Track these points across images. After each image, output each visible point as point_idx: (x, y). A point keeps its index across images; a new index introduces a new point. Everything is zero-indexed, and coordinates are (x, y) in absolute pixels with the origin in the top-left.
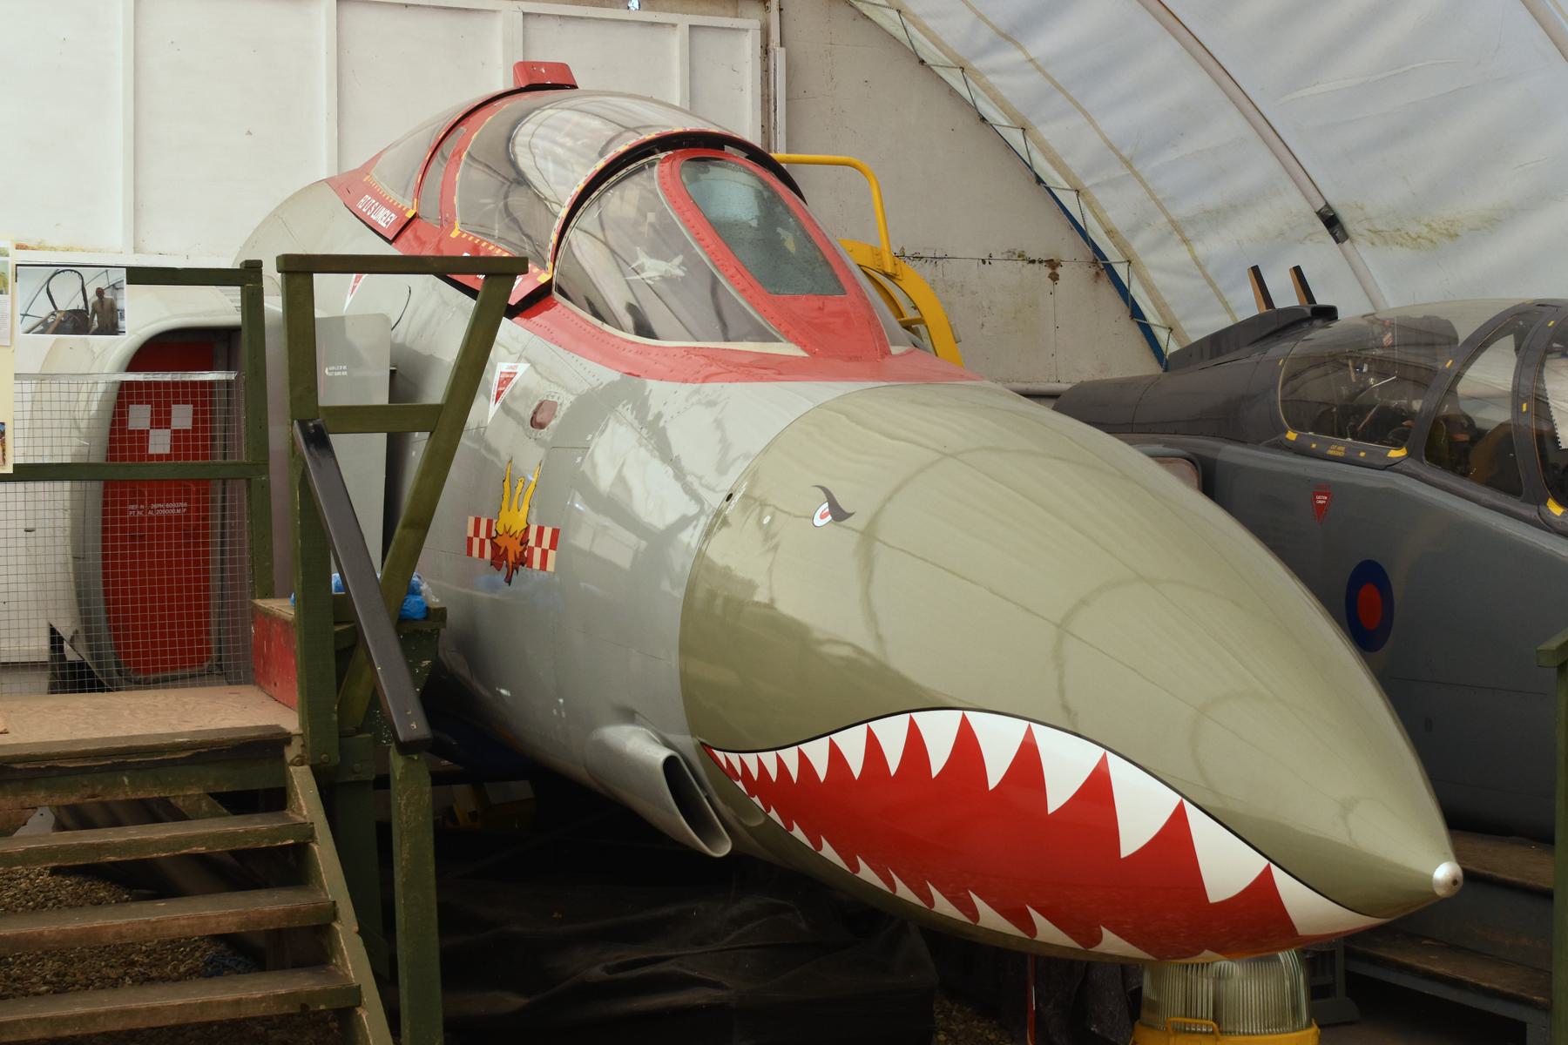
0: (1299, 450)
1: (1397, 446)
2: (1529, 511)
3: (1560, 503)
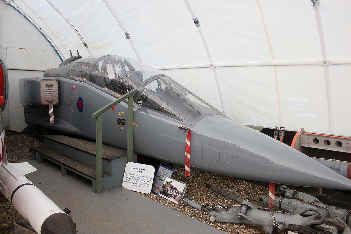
0: (72, 79)
1: (85, 78)
2: (102, 89)
3: (107, 88)
